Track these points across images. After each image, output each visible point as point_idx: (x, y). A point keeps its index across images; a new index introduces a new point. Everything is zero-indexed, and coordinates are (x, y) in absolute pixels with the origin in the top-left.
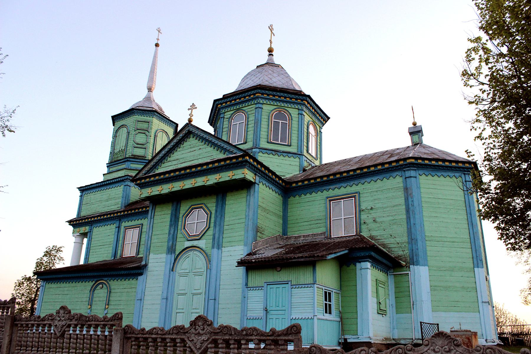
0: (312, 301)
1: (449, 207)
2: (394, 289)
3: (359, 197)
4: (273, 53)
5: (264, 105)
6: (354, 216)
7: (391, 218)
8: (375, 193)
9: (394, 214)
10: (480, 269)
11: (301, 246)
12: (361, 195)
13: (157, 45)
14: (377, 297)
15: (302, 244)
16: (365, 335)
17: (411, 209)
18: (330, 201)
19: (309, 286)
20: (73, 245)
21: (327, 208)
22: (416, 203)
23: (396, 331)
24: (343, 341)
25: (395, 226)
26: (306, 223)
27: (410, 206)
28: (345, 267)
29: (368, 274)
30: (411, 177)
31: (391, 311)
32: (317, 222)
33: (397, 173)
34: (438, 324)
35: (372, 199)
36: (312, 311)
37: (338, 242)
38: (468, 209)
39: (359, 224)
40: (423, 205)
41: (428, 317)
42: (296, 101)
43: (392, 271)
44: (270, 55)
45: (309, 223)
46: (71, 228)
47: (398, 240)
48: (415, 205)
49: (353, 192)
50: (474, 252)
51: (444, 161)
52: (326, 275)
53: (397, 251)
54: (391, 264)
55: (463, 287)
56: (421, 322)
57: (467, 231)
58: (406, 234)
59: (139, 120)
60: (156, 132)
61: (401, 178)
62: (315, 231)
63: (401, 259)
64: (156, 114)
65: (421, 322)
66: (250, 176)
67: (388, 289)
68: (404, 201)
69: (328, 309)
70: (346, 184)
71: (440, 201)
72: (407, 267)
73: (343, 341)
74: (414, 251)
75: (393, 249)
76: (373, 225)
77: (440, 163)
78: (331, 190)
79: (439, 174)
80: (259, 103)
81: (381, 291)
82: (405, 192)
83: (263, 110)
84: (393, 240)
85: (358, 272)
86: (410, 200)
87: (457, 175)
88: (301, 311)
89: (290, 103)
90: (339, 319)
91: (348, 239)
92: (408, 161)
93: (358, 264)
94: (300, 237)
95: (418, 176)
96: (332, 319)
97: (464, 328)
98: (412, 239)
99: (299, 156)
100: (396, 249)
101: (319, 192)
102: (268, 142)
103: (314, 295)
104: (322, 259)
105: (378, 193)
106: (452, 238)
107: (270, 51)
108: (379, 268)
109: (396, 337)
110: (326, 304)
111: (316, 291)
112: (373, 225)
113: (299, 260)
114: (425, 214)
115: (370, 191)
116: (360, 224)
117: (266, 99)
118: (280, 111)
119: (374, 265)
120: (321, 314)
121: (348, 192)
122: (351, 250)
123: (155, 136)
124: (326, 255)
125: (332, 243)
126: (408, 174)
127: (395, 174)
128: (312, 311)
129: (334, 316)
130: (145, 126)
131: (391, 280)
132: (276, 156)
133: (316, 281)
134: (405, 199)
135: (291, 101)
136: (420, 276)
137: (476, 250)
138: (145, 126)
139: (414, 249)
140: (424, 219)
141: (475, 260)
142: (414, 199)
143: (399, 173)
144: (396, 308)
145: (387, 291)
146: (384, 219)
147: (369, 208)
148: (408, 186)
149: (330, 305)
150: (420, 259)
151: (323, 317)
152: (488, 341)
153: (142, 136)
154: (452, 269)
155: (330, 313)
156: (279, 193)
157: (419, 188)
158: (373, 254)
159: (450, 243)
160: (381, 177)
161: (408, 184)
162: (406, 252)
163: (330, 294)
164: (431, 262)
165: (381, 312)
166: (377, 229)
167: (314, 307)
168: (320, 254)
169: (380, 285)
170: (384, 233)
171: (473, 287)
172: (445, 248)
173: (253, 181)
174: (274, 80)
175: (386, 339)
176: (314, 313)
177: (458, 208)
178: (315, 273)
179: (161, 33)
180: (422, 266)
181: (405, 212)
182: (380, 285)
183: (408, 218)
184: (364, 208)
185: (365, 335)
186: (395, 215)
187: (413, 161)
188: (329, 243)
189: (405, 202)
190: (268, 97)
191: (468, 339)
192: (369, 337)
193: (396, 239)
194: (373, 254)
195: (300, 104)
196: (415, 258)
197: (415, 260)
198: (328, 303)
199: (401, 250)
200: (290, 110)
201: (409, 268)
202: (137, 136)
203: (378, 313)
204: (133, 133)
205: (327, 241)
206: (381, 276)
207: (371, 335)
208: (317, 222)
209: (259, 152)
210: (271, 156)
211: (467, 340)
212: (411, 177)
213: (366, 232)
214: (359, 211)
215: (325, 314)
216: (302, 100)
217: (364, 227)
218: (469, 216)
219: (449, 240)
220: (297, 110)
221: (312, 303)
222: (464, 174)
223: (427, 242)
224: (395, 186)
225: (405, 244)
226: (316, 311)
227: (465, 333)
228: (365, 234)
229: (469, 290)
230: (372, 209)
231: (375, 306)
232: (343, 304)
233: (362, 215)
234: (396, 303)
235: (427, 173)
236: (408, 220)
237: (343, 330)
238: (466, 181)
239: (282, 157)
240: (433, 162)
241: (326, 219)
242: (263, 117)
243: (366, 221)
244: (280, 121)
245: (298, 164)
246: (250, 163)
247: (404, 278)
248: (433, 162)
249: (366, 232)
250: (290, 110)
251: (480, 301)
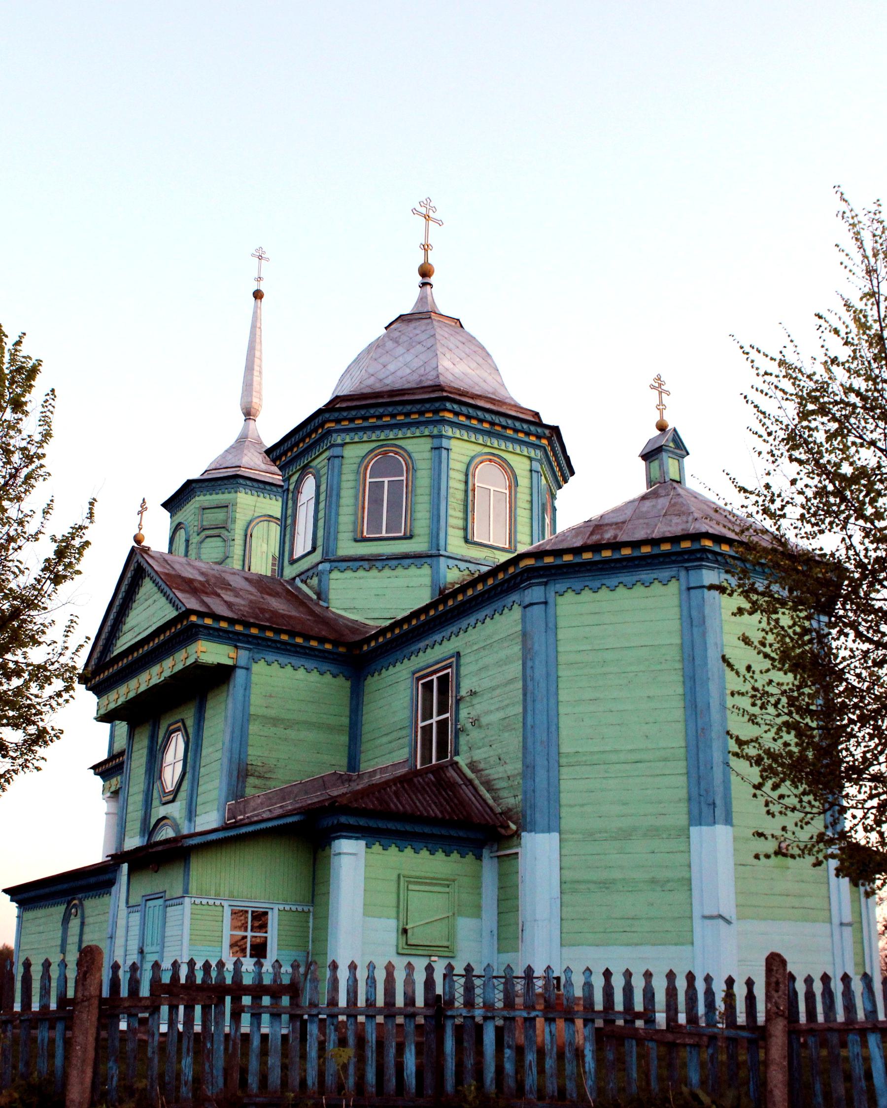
1: (633, 668)
4: (432, 280)
5: (348, 447)
10: (704, 828)
12: (462, 661)
13: (258, 295)
20: (104, 818)
42: (422, 419)
44: (424, 284)
46: (98, 781)
55: (653, 881)
59: (206, 505)
60: (248, 527)
63: (510, 818)
64: (241, 481)
66: (210, 652)
71: (609, 656)
77: (607, 554)
80: (332, 446)
83: (345, 461)
87: (665, 574)
89: (409, 425)
99: (429, 560)
102: (356, 541)
106: (631, 751)
107: (425, 272)
114: (563, 696)
115: (475, 647)
117: (347, 431)
118: (385, 453)
121: (445, 655)
123: (247, 536)
128: (178, 948)
130: (218, 516)
132: (374, 572)
135: (407, 420)
138: (218, 516)
142: (537, 662)
144: (498, 939)
148: (529, 629)
153: (213, 545)
154: (625, 835)
156: (335, 671)
159: (628, 767)
164: (569, 819)
173: (230, 662)
174: (392, 367)
177: (659, 667)
179: (268, 260)
180: (543, 832)
187: (530, 562)
190: (352, 426)
195: (435, 423)
200: (409, 445)
202: (204, 545)
203: (398, 954)
204: (195, 539)
209: (331, 571)
210: (361, 573)
216: (436, 412)
219: (622, 757)
220: (429, 440)
221: (179, 938)
229: (669, 886)
239: (387, 572)
240: (587, 556)
242: (344, 477)
244: (386, 480)
245: (427, 581)
246: (207, 627)
248: (587, 556)
250: (409, 445)
251: (836, 921)
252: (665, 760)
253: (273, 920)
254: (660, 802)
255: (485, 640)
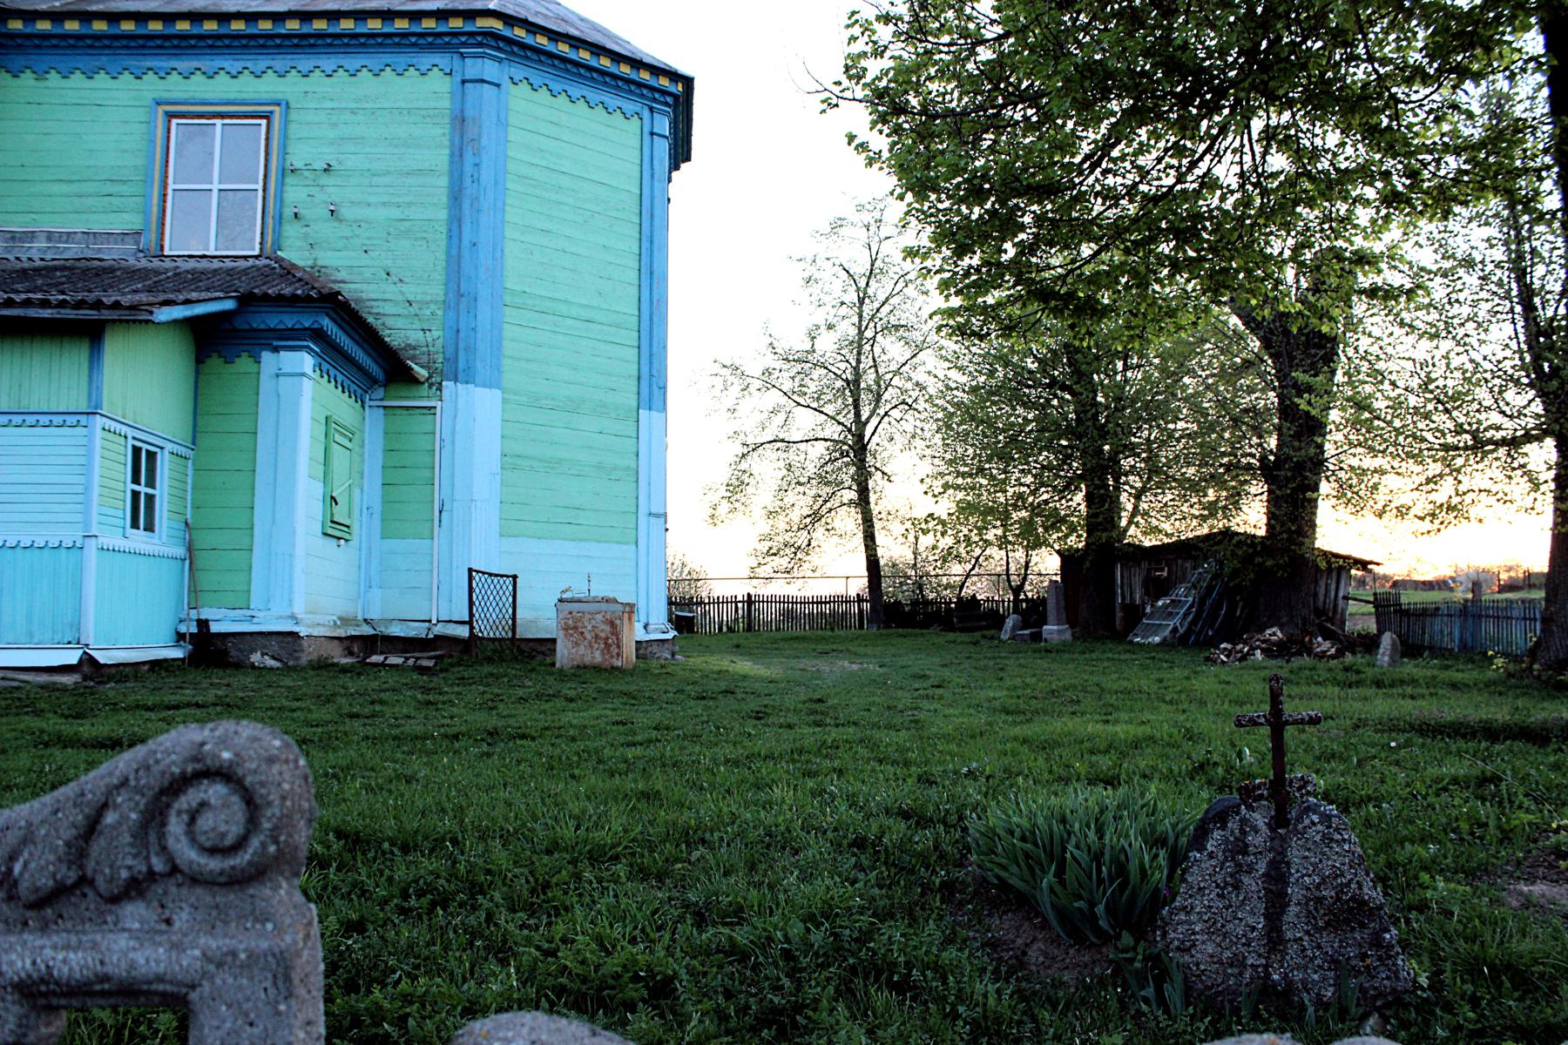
0: (82, 479)
1: (588, 206)
2: (380, 455)
3: (286, 122)
6: (260, 187)
7: (396, 213)
8: (347, 116)
9: (407, 199)
10: (654, 413)
11: (37, 270)
12: (293, 116)
14: (326, 479)
15: (38, 263)
16: (278, 608)
17: (468, 192)
18: (171, 116)
19: (71, 420)
21: (152, 141)
22: (486, 176)
23: (376, 593)
24: (194, 630)
25: (405, 243)
26: (65, 188)
27: (468, 181)
28: (215, 362)
29: (298, 392)
30: (483, 81)
31: (364, 528)
32: (110, 188)
33: (437, 58)
34: (515, 577)
35: (332, 134)
36: (79, 518)
37: (193, 272)
38: (646, 224)
39: (275, 217)
40: (509, 185)
41: (487, 550)
43: (380, 392)
45: (74, 188)
47: (411, 291)
48: (484, 179)
49: (264, 97)
50: (644, 361)
51: (598, 50)
52: (141, 382)
53: (399, 331)
54: (379, 365)
55: (600, 466)
56: (470, 570)
57: (635, 291)
58: (439, 277)
61: (448, 78)
62: (100, 224)
63: (413, 358)
65: (470, 570)
67: (362, 455)
68: (446, 159)
69: (141, 513)
70: (239, 65)
72: (431, 386)
73: (194, 630)
74: (462, 335)
75: (390, 322)
76: (325, 229)
77: (584, 55)
78: (174, 76)
79: (575, 91)
81: (339, 457)
82: (453, 130)
84: (392, 288)
85: (266, 383)
86: (469, 159)
87: (630, 107)
88: (25, 517)
90: (180, 551)
91: (229, 264)
92: (483, 23)
93: (266, 356)
94: (32, 236)
95: (506, 83)
96: (156, 549)
97: (599, 590)
98: (459, 294)
100: (400, 323)
101: (127, 76)
103: (89, 455)
104: (134, 318)
105: (359, 118)
108: (340, 378)
109: (374, 615)
110: (135, 495)
111: (98, 442)
112: (325, 229)
113: (33, 313)
114: (511, 215)
115: (330, 105)
116: (280, 219)
119: (325, 366)
120: (115, 532)
121: (244, 96)
122: (247, 301)
124: (152, 304)
125: (167, 270)
126: (474, 67)
127: (426, 60)
129: (164, 540)
131: (372, 425)
133: (99, 405)
134: (452, 155)
136: (472, 417)
137: (651, 356)
139: (462, 326)
140: (508, 234)
141: (644, 383)
142: (485, 158)
143: (443, 60)
145: (356, 458)
146: (370, 213)
147: (321, 165)
148: (469, 113)
149: (150, 499)
150: (479, 365)
151: (120, 543)
152: (651, 627)
155: (150, 528)
157: (502, 123)
158: (326, 323)
160: (374, 61)
161: (468, 105)
162: (436, 334)
163: (151, 456)
165: (336, 530)
166: (340, 244)
167: (87, 504)
168: (126, 300)
169: (338, 438)
170: (364, 260)
171: (628, 468)
172: (561, 337)
175: (345, 621)
176: (87, 524)
177: (615, 214)
178: (100, 370)
180: (485, 386)
181: (444, 199)
182: (338, 438)
183: (455, 222)
184: (298, 164)
185: (278, 608)
186: (410, 204)
187: (497, 25)
188: (157, 272)
189: (451, 163)
191: (612, 624)
192: (293, 617)
193: (404, 288)
194: (326, 323)
196: (462, 355)
197: (461, 365)
198: (142, 489)
199: (418, 325)
201: (440, 389)
203: (325, 534)
205: (144, 263)
206: (343, 406)
207: (299, 609)
208: (110, 188)
211: (608, 628)
212: (483, 81)
213: (300, 249)
214: (279, 172)
215: (130, 531)
217: (291, 231)
218: (645, 245)
219: (574, 311)
222: (651, 109)
223: (507, 311)
224: (420, 104)
225: (433, 307)
226: (95, 518)
227: (604, 606)
228: (295, 254)
230: (328, 169)
231: (317, 508)
232: (193, 493)
233: (288, 188)
234: (386, 502)
235: (536, 81)
236: (455, 228)
237: (194, 590)
238: (652, 134)
241: (148, 181)
243: (302, 212)
247: (419, 422)
249: (300, 249)
252: (618, 326)
253: (164, 465)
254: (610, 375)
255: (358, 100)
